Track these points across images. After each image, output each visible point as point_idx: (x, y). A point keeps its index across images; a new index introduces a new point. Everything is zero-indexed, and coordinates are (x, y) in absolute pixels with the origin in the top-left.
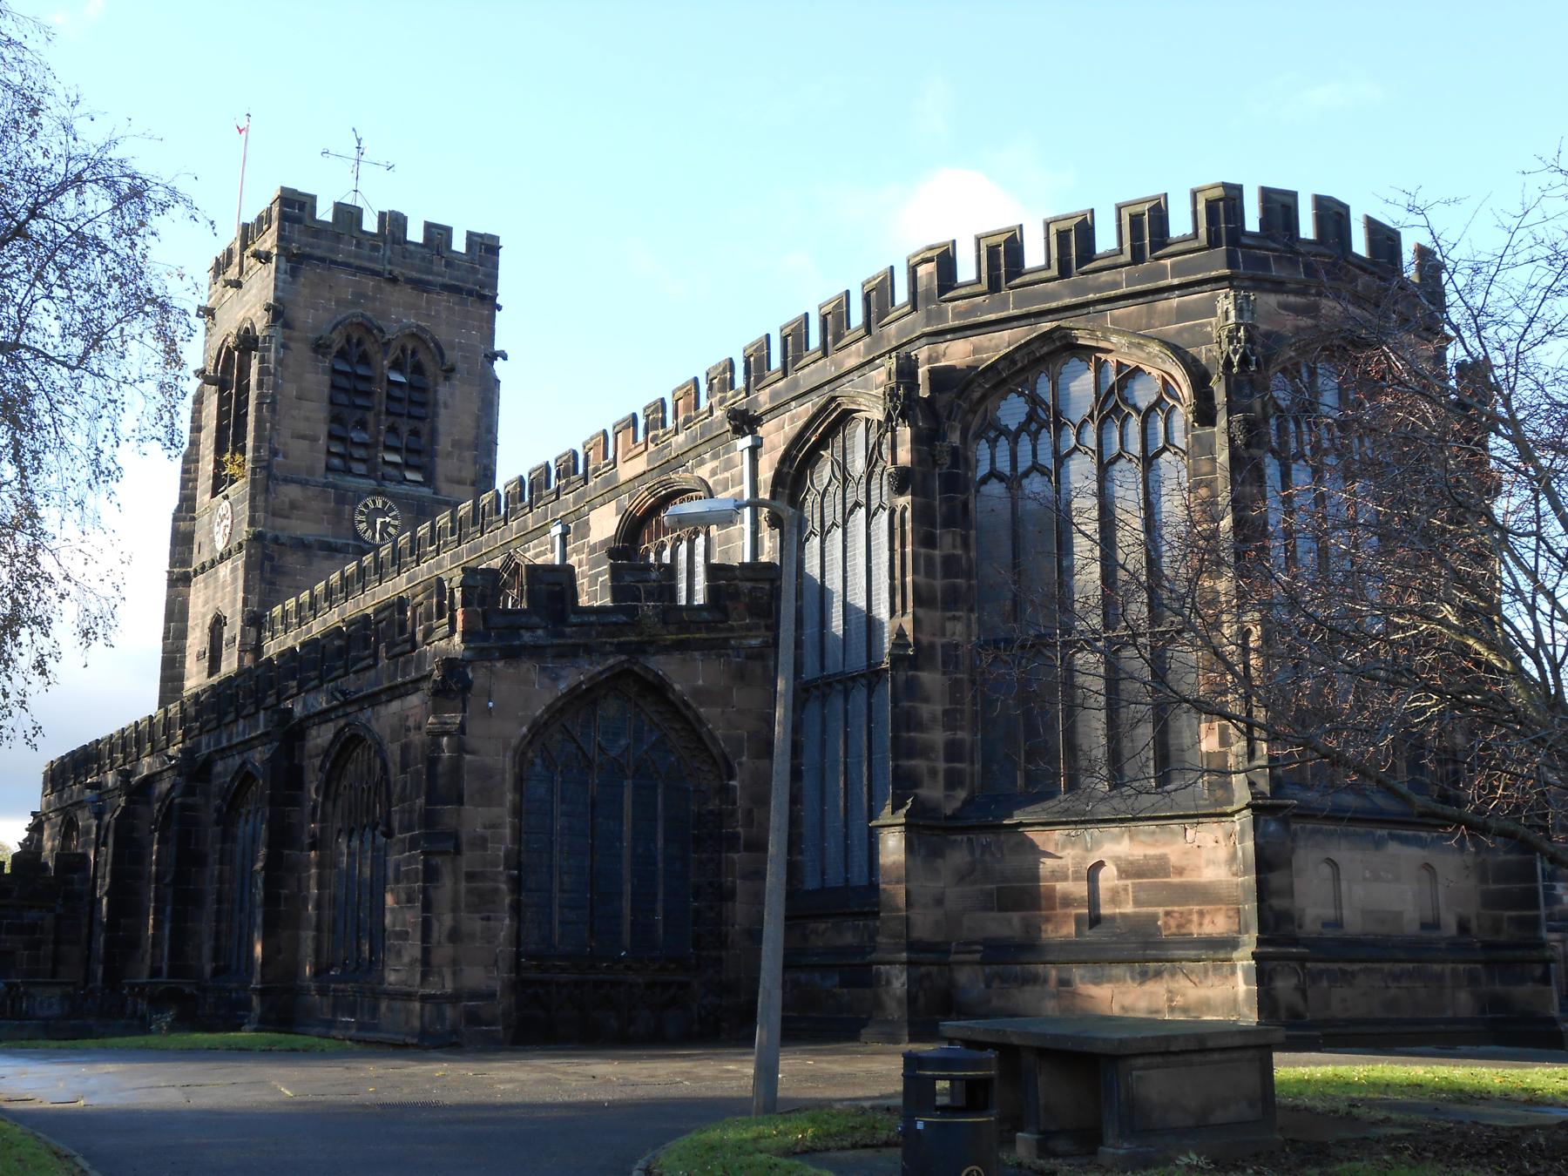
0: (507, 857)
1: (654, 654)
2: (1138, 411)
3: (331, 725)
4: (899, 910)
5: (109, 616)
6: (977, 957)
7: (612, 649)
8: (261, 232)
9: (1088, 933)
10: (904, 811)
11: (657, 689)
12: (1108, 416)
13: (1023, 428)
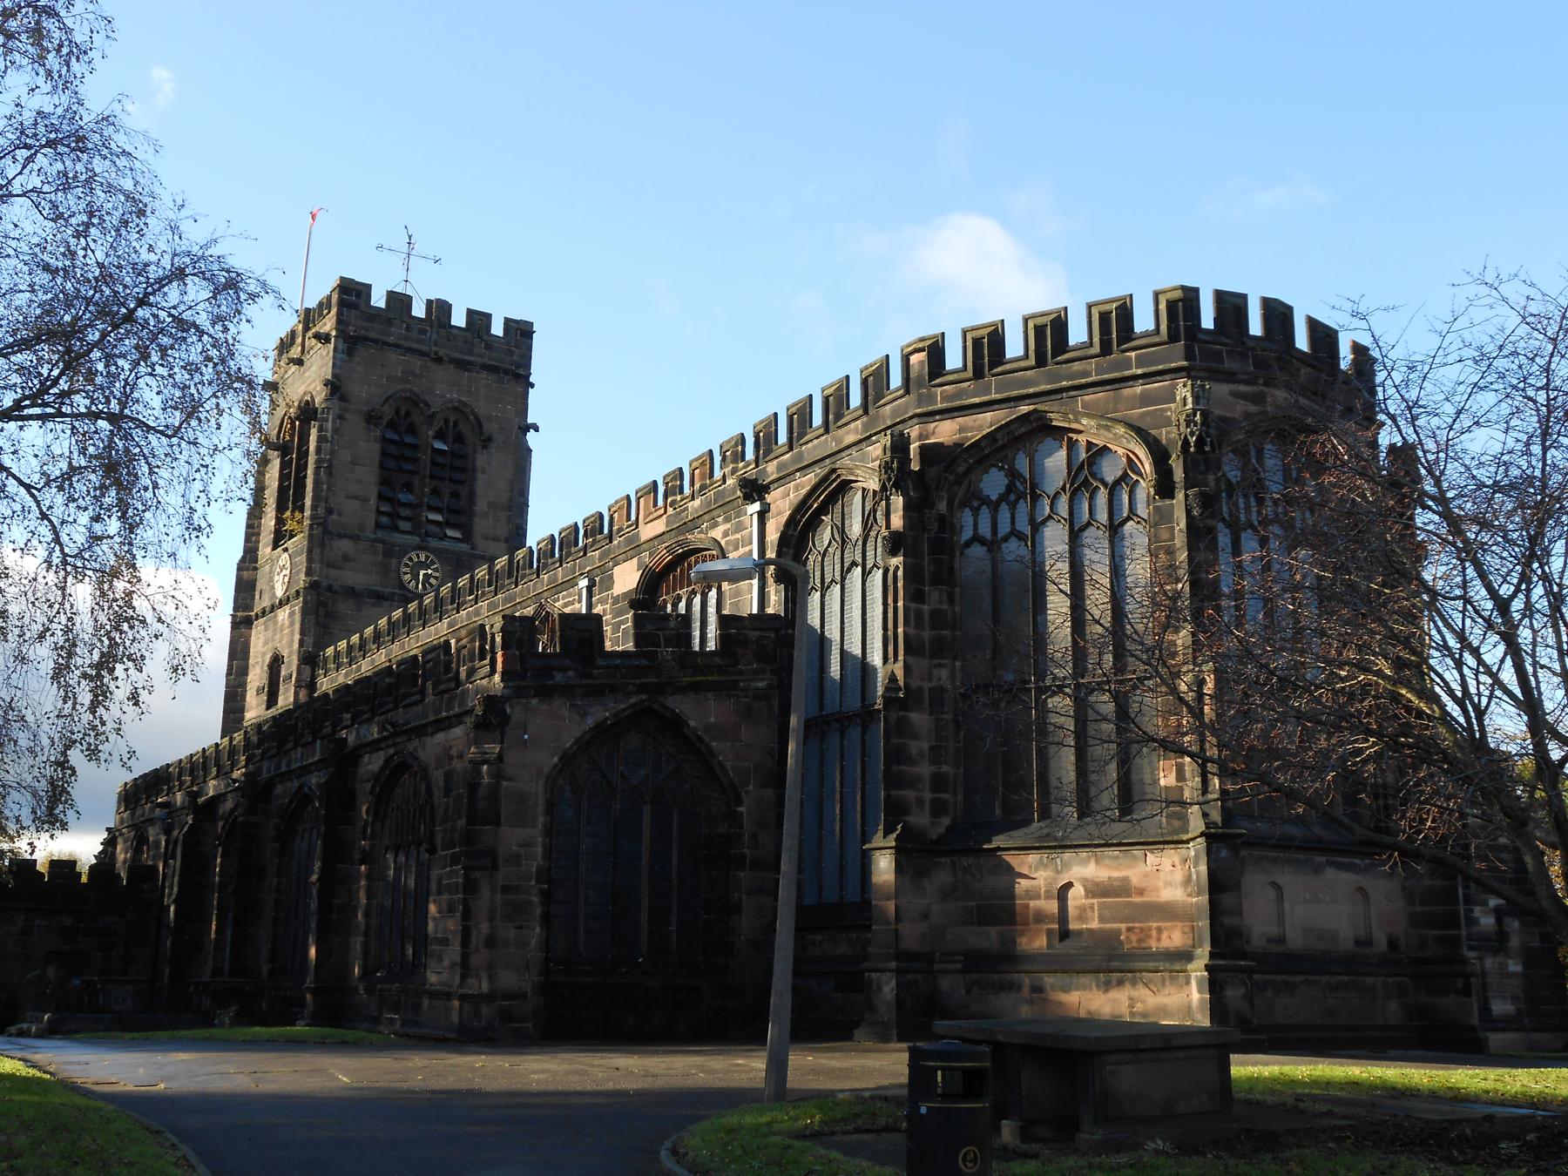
0: (538, 872)
2: (1105, 484)
3: (382, 753)
11: (675, 725)
12: (1078, 489)
13: (1003, 498)
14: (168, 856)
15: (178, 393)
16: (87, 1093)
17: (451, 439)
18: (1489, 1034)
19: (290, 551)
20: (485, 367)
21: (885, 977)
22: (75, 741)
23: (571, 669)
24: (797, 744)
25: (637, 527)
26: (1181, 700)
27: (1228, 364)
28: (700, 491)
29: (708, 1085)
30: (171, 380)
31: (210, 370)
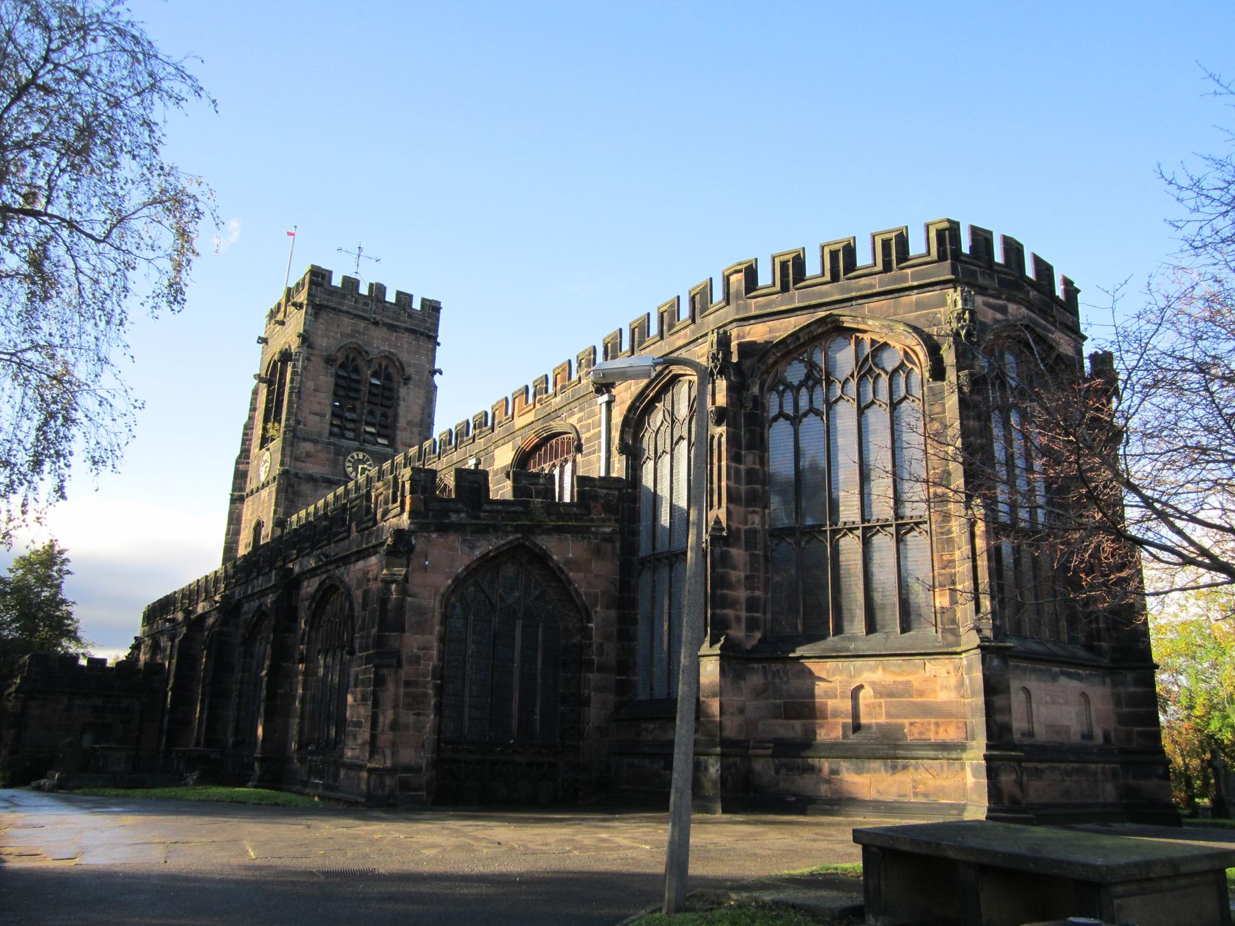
1: (540, 534)
2: (887, 373)
3: (317, 578)
4: (715, 716)
5: (116, 448)
6: (769, 752)
7: (512, 529)
8: (298, 291)
9: (852, 736)
10: (719, 645)
11: (542, 558)
12: (864, 375)
13: (802, 384)
20: (407, 330)
21: (712, 760)
27: (981, 280)
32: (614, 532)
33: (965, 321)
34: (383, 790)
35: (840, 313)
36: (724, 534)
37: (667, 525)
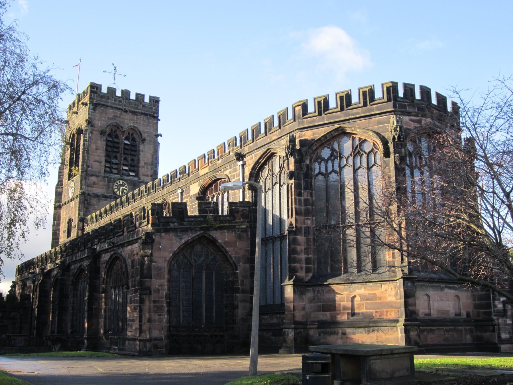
0: (166, 295)
1: (212, 231)
2: (366, 153)
3: (109, 253)
6: (316, 326)
10: (292, 280)
11: (213, 242)
13: (329, 158)
14: (34, 291)
15: (36, 125)
16: (11, 375)
17: (131, 140)
18: (501, 345)
19: (74, 181)
21: (290, 330)
22: (2, 251)
23: (175, 222)
24: (259, 248)
25: (198, 171)
26: (395, 230)
27: (408, 109)
28: (221, 157)
29: (229, 370)
30: (34, 121)
31: (48, 117)
32: (247, 227)
33: (397, 131)
34: (146, 349)
35: (344, 126)
36: (294, 230)
37: (271, 224)
